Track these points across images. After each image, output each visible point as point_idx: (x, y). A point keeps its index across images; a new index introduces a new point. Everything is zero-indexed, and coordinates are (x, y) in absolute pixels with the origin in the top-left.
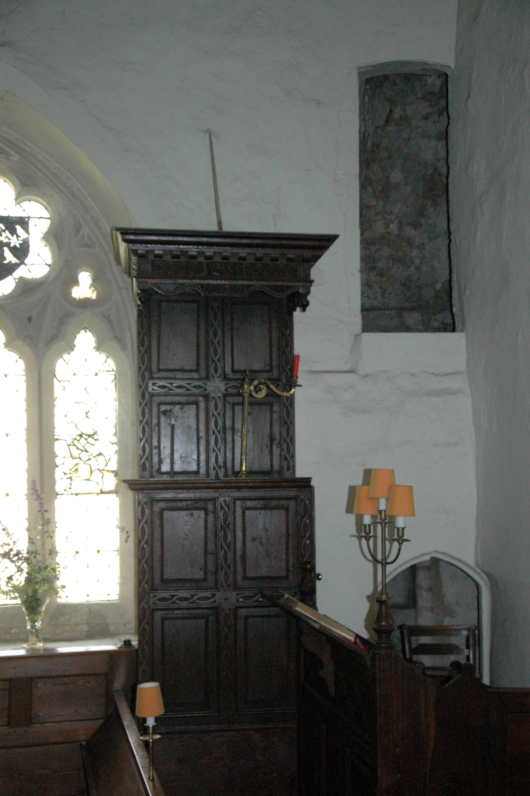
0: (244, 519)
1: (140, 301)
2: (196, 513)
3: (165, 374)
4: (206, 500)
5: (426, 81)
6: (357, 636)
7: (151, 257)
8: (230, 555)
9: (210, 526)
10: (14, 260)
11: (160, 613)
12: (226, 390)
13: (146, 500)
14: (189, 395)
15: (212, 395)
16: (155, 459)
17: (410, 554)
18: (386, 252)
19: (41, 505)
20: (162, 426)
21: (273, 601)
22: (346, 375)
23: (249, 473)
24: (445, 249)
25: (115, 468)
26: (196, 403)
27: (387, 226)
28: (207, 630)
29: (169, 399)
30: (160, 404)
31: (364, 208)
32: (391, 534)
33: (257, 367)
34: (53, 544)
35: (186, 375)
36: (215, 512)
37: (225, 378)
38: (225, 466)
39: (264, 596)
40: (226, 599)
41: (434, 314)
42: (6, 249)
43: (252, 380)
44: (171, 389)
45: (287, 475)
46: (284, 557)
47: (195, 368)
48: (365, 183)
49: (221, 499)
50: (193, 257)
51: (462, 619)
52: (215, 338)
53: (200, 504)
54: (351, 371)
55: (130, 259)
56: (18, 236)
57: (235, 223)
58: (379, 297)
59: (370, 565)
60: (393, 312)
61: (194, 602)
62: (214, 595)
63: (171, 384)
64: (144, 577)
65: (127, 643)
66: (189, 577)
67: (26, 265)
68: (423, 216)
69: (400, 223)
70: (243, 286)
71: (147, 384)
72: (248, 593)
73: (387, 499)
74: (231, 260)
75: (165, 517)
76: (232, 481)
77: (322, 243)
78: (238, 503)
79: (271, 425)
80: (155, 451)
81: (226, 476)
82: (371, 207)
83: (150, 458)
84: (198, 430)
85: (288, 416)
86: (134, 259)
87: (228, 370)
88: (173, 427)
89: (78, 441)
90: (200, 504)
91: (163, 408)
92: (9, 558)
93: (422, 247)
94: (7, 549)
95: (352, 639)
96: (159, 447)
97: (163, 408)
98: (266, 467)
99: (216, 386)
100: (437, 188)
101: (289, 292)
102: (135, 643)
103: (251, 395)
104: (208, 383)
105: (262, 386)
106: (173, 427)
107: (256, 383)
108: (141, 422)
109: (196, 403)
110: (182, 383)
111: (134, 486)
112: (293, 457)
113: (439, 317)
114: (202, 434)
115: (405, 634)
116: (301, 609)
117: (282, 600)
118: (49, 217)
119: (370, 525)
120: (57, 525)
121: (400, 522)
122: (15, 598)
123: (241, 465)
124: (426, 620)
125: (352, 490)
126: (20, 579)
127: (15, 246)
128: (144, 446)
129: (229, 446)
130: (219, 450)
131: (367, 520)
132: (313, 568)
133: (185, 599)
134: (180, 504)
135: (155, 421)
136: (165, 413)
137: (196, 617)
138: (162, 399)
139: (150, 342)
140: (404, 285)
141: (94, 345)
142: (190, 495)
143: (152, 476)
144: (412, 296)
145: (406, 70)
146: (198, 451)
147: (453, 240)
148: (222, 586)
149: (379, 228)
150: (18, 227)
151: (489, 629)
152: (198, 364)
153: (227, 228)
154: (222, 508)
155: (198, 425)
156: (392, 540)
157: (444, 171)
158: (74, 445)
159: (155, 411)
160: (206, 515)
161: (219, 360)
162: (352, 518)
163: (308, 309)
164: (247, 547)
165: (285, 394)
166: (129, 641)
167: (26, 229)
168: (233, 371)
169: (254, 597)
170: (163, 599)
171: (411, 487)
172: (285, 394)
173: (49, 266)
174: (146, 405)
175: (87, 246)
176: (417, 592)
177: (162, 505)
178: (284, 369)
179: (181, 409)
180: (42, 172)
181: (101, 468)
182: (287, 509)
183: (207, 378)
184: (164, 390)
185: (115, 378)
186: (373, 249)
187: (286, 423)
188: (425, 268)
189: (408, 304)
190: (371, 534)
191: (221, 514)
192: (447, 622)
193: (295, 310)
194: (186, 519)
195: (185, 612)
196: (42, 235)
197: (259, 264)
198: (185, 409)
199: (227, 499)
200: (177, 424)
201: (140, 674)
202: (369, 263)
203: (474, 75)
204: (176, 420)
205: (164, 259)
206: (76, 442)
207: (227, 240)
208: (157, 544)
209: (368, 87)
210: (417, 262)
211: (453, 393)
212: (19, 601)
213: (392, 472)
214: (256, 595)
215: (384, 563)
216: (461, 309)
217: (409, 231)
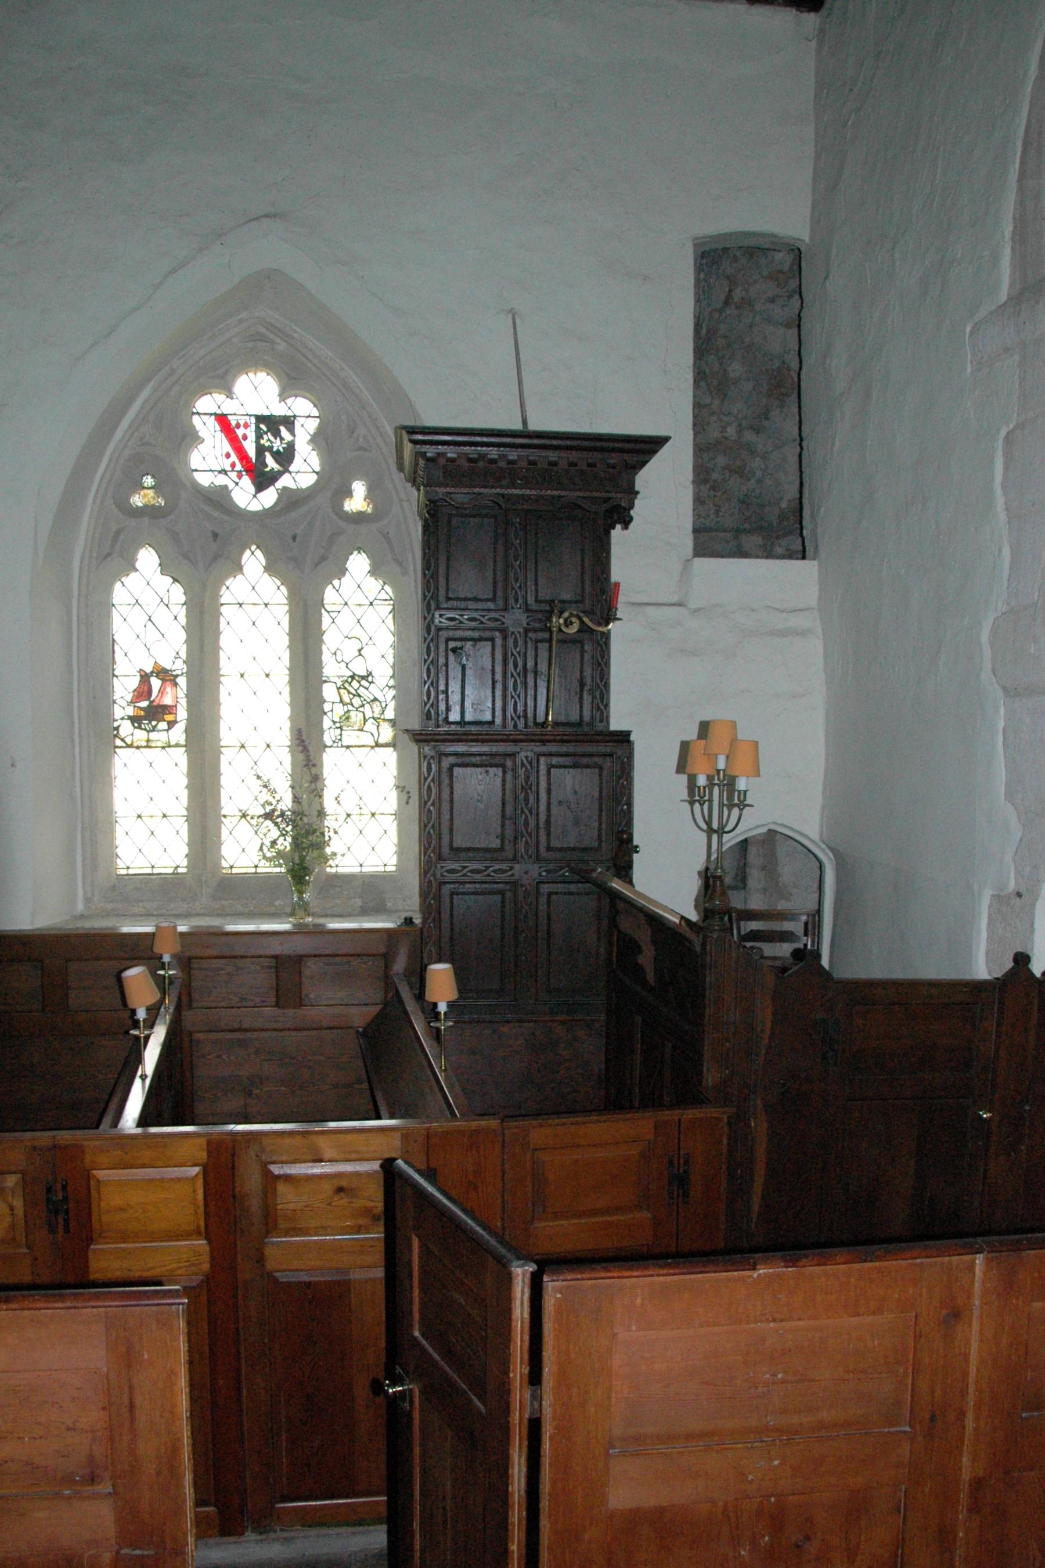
0: (549, 779)
1: (429, 514)
2: (492, 770)
3: (455, 603)
4: (506, 755)
5: (773, 257)
6: (682, 918)
7: (442, 461)
8: (532, 822)
9: (509, 786)
10: (276, 467)
11: (448, 886)
12: (528, 624)
13: (432, 753)
14: (485, 629)
15: (511, 629)
16: (442, 707)
17: (751, 823)
18: (721, 461)
19: (308, 758)
20: (450, 667)
21: (583, 876)
22: (672, 608)
23: (556, 724)
24: (793, 460)
25: (392, 717)
26: (492, 640)
27: (723, 429)
28: (503, 906)
29: (459, 634)
30: (448, 640)
31: (697, 406)
32: (730, 797)
33: (567, 596)
34: (321, 804)
35: (480, 605)
36: (514, 770)
37: (527, 610)
38: (525, 716)
39: (572, 870)
40: (526, 873)
41: (777, 538)
42: (267, 454)
43: (561, 613)
44: (461, 622)
45: (600, 727)
46: (596, 824)
47: (491, 596)
48: (700, 376)
49: (523, 755)
50: (493, 461)
51: (801, 902)
52: (516, 560)
53: (497, 760)
54: (680, 604)
55: (417, 464)
56: (282, 439)
57: (545, 419)
58: (712, 516)
59: (704, 836)
60: (729, 535)
61: (489, 875)
62: (512, 868)
63: (462, 615)
64: (430, 844)
65: (409, 921)
66: (483, 846)
67: (290, 473)
68: (767, 419)
69: (740, 425)
70: (553, 497)
71: (433, 615)
72: (551, 866)
73: (727, 757)
74: (539, 466)
75: (455, 774)
76: (538, 734)
77: (646, 447)
78: (542, 759)
79: (582, 664)
80: (441, 697)
81: (526, 726)
82: (704, 406)
83: (435, 705)
84: (493, 674)
85: (603, 657)
86: (422, 462)
87: (531, 600)
88: (464, 667)
89: (350, 684)
90: (497, 760)
91: (452, 644)
92: (271, 820)
93: (764, 457)
94: (268, 808)
95: (677, 921)
96: (446, 692)
97: (452, 644)
98: (575, 717)
99: (516, 619)
100: (785, 385)
101: (606, 506)
102: (418, 921)
103: (560, 630)
104: (506, 615)
105: (573, 619)
106: (464, 667)
107: (566, 615)
108: (425, 661)
109: (492, 640)
110: (475, 615)
111: (420, 738)
112: (607, 706)
113: (784, 542)
114: (499, 676)
115: (734, 918)
116: (616, 885)
117: (594, 875)
118: (317, 414)
119: (704, 788)
120: (326, 783)
121: (742, 784)
122: (280, 866)
123: (547, 714)
124: (756, 903)
125: (685, 746)
126: (285, 844)
127: (278, 450)
128: (429, 691)
129: (530, 692)
130: (519, 696)
131: (702, 781)
132: (630, 839)
133: (478, 872)
134: (473, 760)
135: (442, 660)
136: (454, 650)
137: (490, 893)
138: (451, 633)
139: (437, 565)
140: (743, 502)
141: (368, 568)
142: (485, 748)
143: (438, 726)
144: (755, 515)
145: (752, 242)
146: (494, 697)
147: (805, 448)
148: (522, 857)
149: (714, 433)
150: (282, 429)
151: (832, 916)
152: (495, 595)
153: (533, 426)
154: (523, 765)
155: (493, 666)
156: (731, 806)
157: (795, 365)
158: (345, 688)
159: (442, 648)
160: (504, 772)
161: (520, 587)
162: (684, 779)
163: (631, 526)
164: (552, 812)
165: (600, 629)
166: (411, 919)
167: (292, 431)
168: (537, 601)
169: (558, 871)
170: (452, 871)
171: (757, 742)
172: (600, 629)
173: (317, 473)
174: (432, 640)
175: (361, 448)
176: (748, 870)
177: (452, 760)
178: (600, 601)
179: (474, 646)
180: (311, 361)
181: (377, 715)
182: (601, 768)
183: (505, 609)
184: (452, 623)
185: (393, 609)
186: (706, 457)
187: (599, 664)
188: (768, 482)
189: (747, 526)
190: (706, 798)
191: (521, 772)
192: (782, 905)
193: (614, 528)
194: (480, 777)
195: (478, 886)
196: (309, 437)
197: (573, 469)
198: (478, 646)
199: (529, 754)
200: (469, 665)
202: (702, 474)
203: (834, 251)
204: (467, 660)
205: (458, 463)
206: (347, 685)
207: (536, 441)
208: (446, 806)
209: (704, 261)
210: (759, 474)
211: (803, 633)
212: (283, 870)
213: (734, 724)
214: (562, 868)
215: (721, 831)
216: (814, 531)
217: (749, 436)
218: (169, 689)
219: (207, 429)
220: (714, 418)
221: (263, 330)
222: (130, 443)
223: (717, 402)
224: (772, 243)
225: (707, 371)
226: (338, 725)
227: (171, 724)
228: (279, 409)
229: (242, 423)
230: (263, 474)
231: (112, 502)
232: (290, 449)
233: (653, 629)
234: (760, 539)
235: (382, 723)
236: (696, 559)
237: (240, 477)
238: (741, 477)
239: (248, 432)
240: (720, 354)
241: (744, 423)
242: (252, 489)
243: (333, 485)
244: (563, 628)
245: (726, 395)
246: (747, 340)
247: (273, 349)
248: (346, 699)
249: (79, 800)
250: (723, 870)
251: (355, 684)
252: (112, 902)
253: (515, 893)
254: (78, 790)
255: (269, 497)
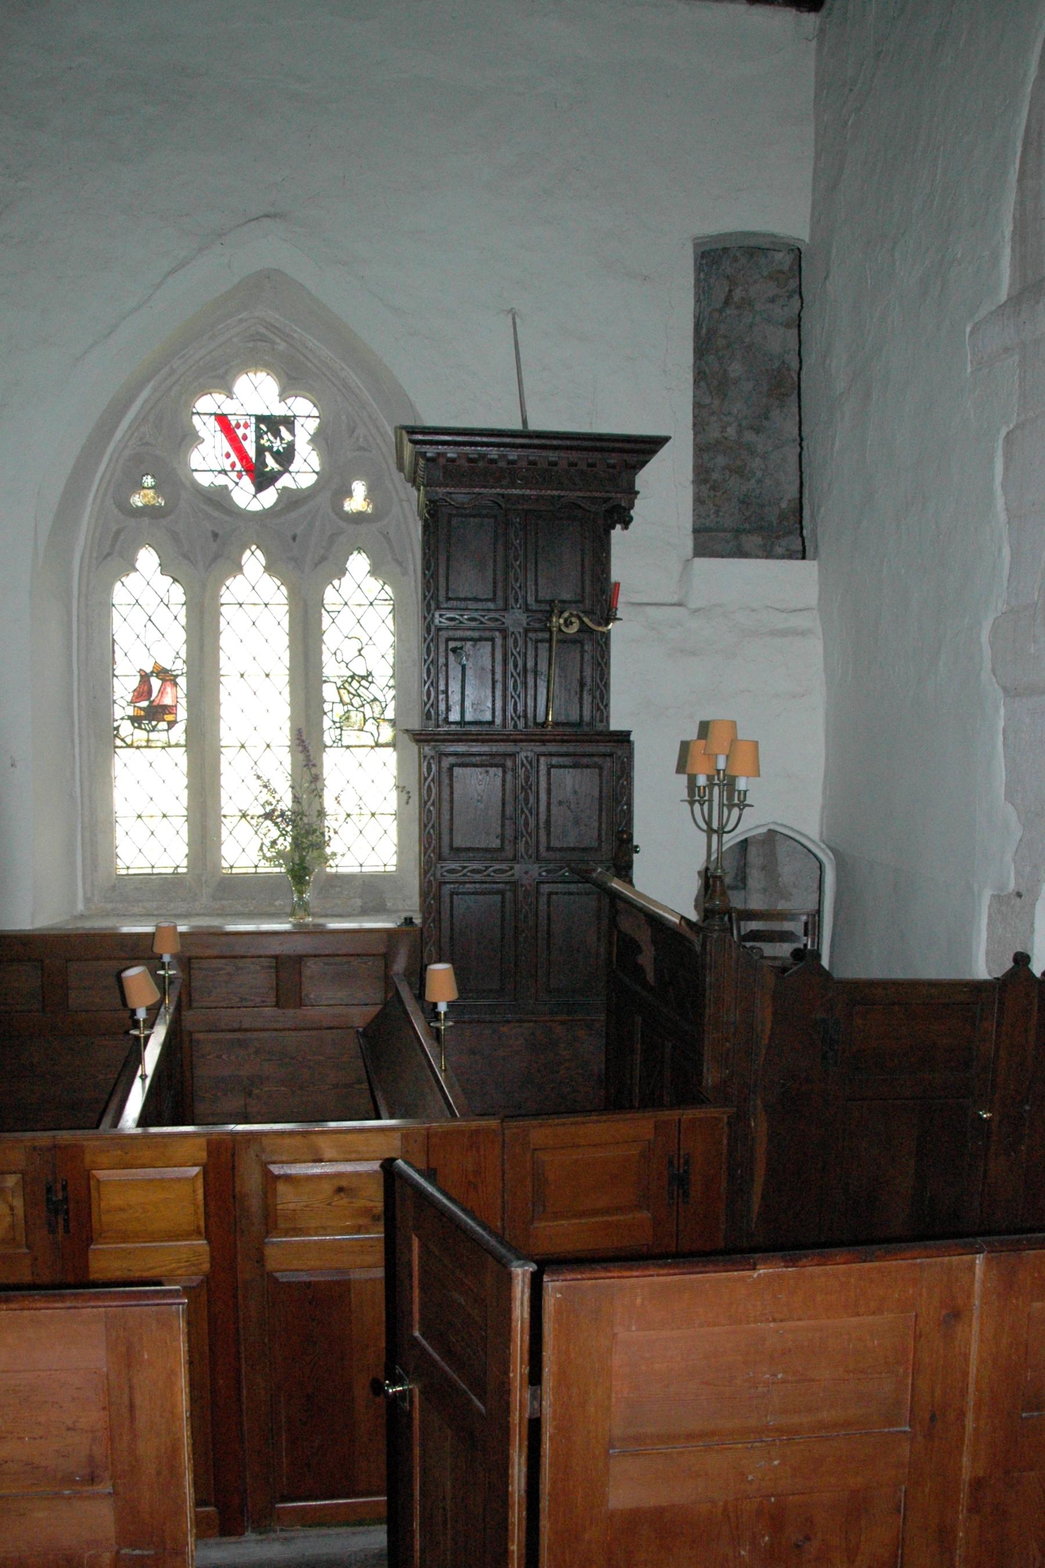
0: (549, 779)
1: (429, 514)
2: (492, 770)
3: (455, 603)
4: (506, 755)
5: (773, 257)
6: (682, 918)
7: (442, 461)
8: (532, 822)
9: (509, 786)
10: (276, 467)
11: (448, 886)
12: (528, 624)
13: (432, 753)
14: (485, 629)
15: (511, 629)
16: (442, 707)
17: (751, 823)
18: (721, 461)
19: (308, 758)
20: (450, 667)
21: (583, 876)
22: (672, 608)
23: (556, 724)
24: (793, 460)
25: (392, 717)
26: (492, 640)
27: (723, 429)
28: (503, 906)
29: (459, 634)
30: (448, 640)
31: (697, 406)
32: (730, 797)
33: (567, 596)
34: (321, 804)
35: (480, 605)
36: (514, 770)
37: (527, 610)
38: (525, 716)
39: (572, 870)
40: (526, 873)
41: (777, 538)
42: (267, 454)
43: (561, 613)
44: (461, 622)
45: (600, 727)
46: (596, 824)
47: (491, 596)
48: (700, 376)
49: (523, 755)
50: (493, 461)
51: (801, 902)
52: (516, 560)
53: (497, 760)
54: (680, 604)
55: (417, 464)
56: (282, 439)
57: (545, 419)
58: (712, 516)
59: (704, 836)
60: (729, 535)
61: (489, 875)
62: (512, 868)
63: (462, 615)
64: (430, 844)
65: (409, 921)
66: (483, 846)
67: (290, 473)
68: (767, 419)
69: (740, 425)
70: (553, 497)
71: (433, 615)
72: (551, 866)
73: (727, 757)
74: (539, 466)
75: (455, 774)
76: (538, 734)
77: (646, 447)
78: (542, 759)
79: (582, 664)
80: (441, 697)
81: (526, 726)
82: (704, 406)
83: (435, 705)
84: (493, 674)
85: (603, 657)
86: (422, 462)
87: (531, 600)
88: (464, 667)
89: (350, 684)
90: (497, 760)
91: (452, 644)
92: (271, 820)
93: (764, 457)
94: (268, 808)
95: (677, 921)
96: (446, 692)
97: (452, 644)
98: (575, 717)
99: (516, 619)
100: (785, 385)
101: (606, 506)
102: (418, 921)
103: (560, 630)
104: (506, 615)
105: (573, 619)
106: (464, 667)
107: (566, 615)
108: (425, 661)
109: (492, 640)
110: (475, 615)
111: (420, 738)
112: (607, 706)
113: (784, 542)
114: (499, 676)
115: (734, 918)
116: (616, 885)
117: (594, 875)
118: (317, 414)
119: (704, 788)
120: (326, 783)
121: (742, 784)
122: (280, 866)
123: (547, 714)
124: (756, 903)
125: (685, 746)
126: (285, 844)
127: (278, 450)
128: (429, 691)
129: (530, 692)
130: (519, 696)
131: (702, 781)
132: (630, 839)
133: (478, 872)
134: (473, 760)
135: (442, 660)
136: (454, 650)
137: (490, 893)
138: (451, 633)
139: (437, 565)
140: (743, 502)
141: (368, 568)
142: (485, 748)
143: (438, 726)
144: (755, 515)
145: (752, 242)
146: (494, 697)
147: (805, 448)
148: (522, 857)
149: (714, 433)
150: (282, 429)
151: (832, 916)
152: (495, 595)
153: (533, 426)
154: (523, 765)
155: (493, 666)
156: (731, 806)
157: (795, 365)
158: (345, 688)
159: (442, 648)
160: (504, 772)
161: (520, 587)
162: (684, 779)
163: (631, 526)
164: (552, 812)
165: (600, 629)
166: (411, 919)
167: (292, 431)
168: (537, 601)
169: (558, 871)
170: (452, 871)
171: (757, 742)
172: (600, 629)
173: (317, 473)
174: (432, 640)
175: (361, 448)
176: (748, 870)
177: (452, 760)
178: (600, 601)
179: (474, 646)
180: (311, 361)
181: (377, 715)
182: (601, 768)
183: (505, 609)
184: (452, 623)
185: (393, 609)
186: (706, 457)
187: (599, 664)
188: (768, 482)
189: (747, 526)
190: (706, 798)
191: (521, 772)
192: (782, 905)
193: (614, 528)
194: (480, 777)
195: (478, 886)
196: (309, 437)
197: (573, 469)
198: (478, 646)
199: (529, 754)
200: (469, 665)
201: (425, 955)
202: (702, 474)
203: (834, 251)
204: (467, 660)
205: (458, 463)
206: (347, 685)
207: (536, 441)
208: (446, 806)
209: (704, 261)
210: (759, 474)
211: (803, 633)
212: (283, 870)
213: (734, 724)
214: (562, 868)
215: (721, 831)
216: (814, 531)
217: (749, 436)
218: (169, 689)
219: (207, 429)
220: (714, 418)
221: (263, 330)
222: (130, 443)
223: (717, 402)
224: (772, 243)
225: (707, 371)
226: (338, 725)
227: (171, 724)
228: (279, 409)
229: (242, 423)
230: (263, 474)
231: (112, 502)
232: (290, 449)
233: (653, 629)
234: (760, 539)
235: (382, 723)
236: (696, 559)
237: (240, 477)
238: (741, 477)
239: (248, 432)
240: (720, 354)
241: (744, 423)
242: (252, 489)
243: (333, 485)
244: (563, 628)
245: (726, 395)
246: (747, 340)
247: (273, 349)
248: (346, 699)
249: (79, 800)
250: (723, 870)
251: (355, 684)
252: (112, 902)
253: (515, 893)
254: (78, 790)
255: (269, 497)
